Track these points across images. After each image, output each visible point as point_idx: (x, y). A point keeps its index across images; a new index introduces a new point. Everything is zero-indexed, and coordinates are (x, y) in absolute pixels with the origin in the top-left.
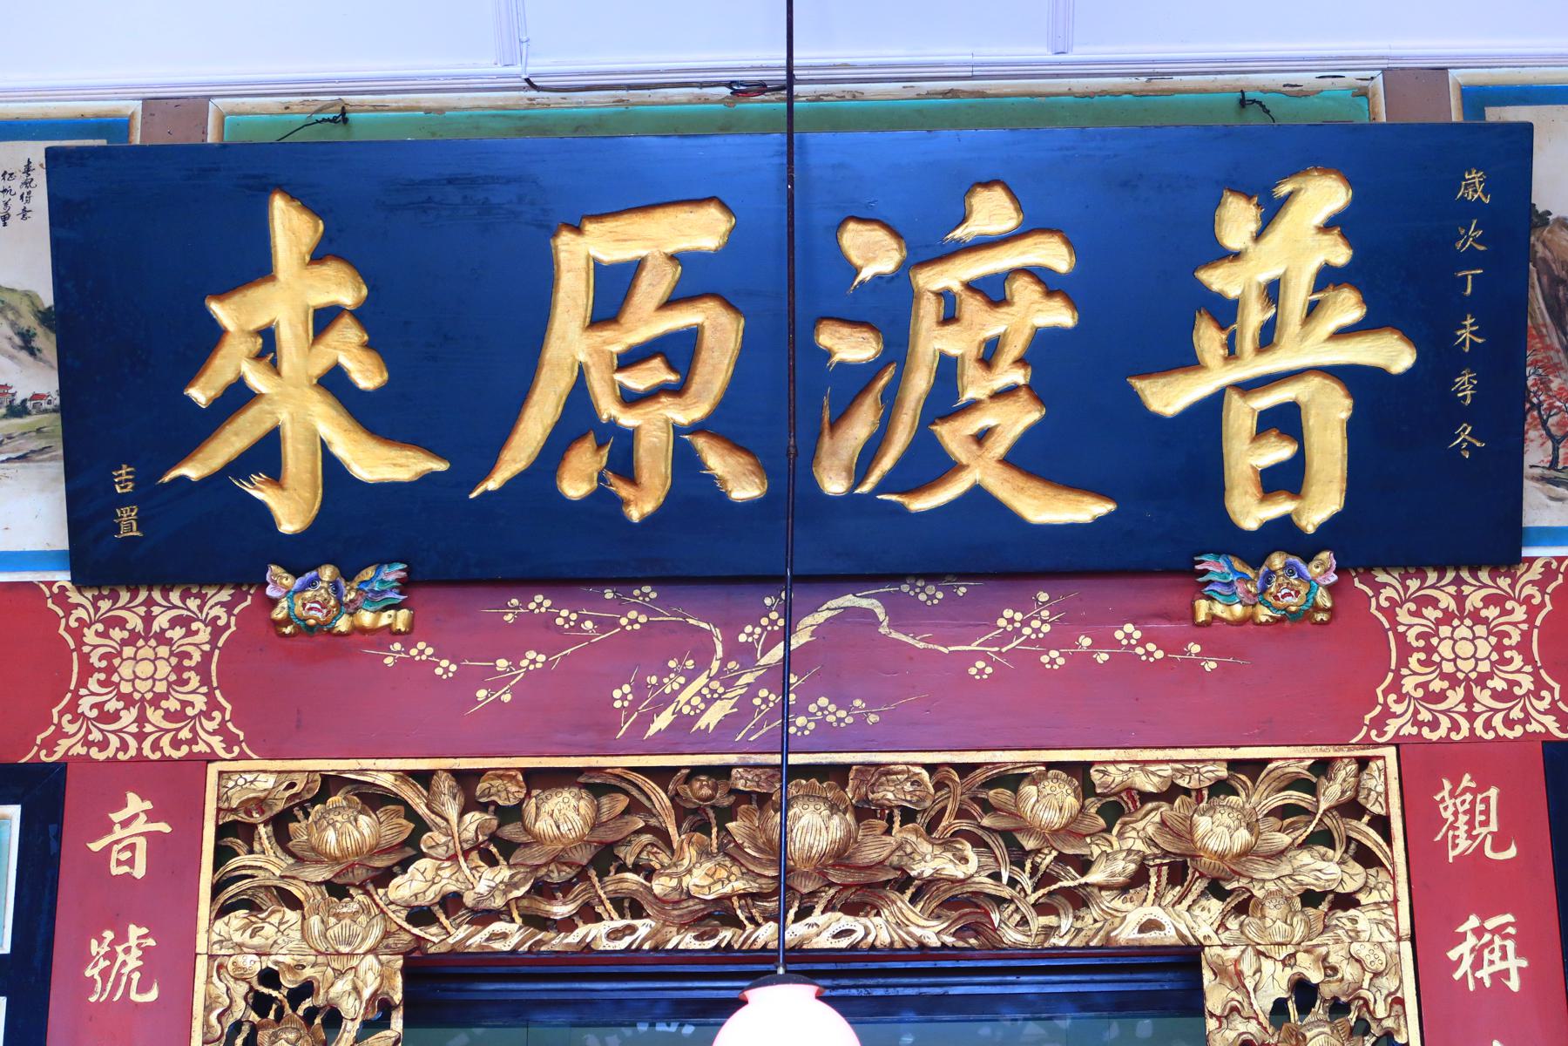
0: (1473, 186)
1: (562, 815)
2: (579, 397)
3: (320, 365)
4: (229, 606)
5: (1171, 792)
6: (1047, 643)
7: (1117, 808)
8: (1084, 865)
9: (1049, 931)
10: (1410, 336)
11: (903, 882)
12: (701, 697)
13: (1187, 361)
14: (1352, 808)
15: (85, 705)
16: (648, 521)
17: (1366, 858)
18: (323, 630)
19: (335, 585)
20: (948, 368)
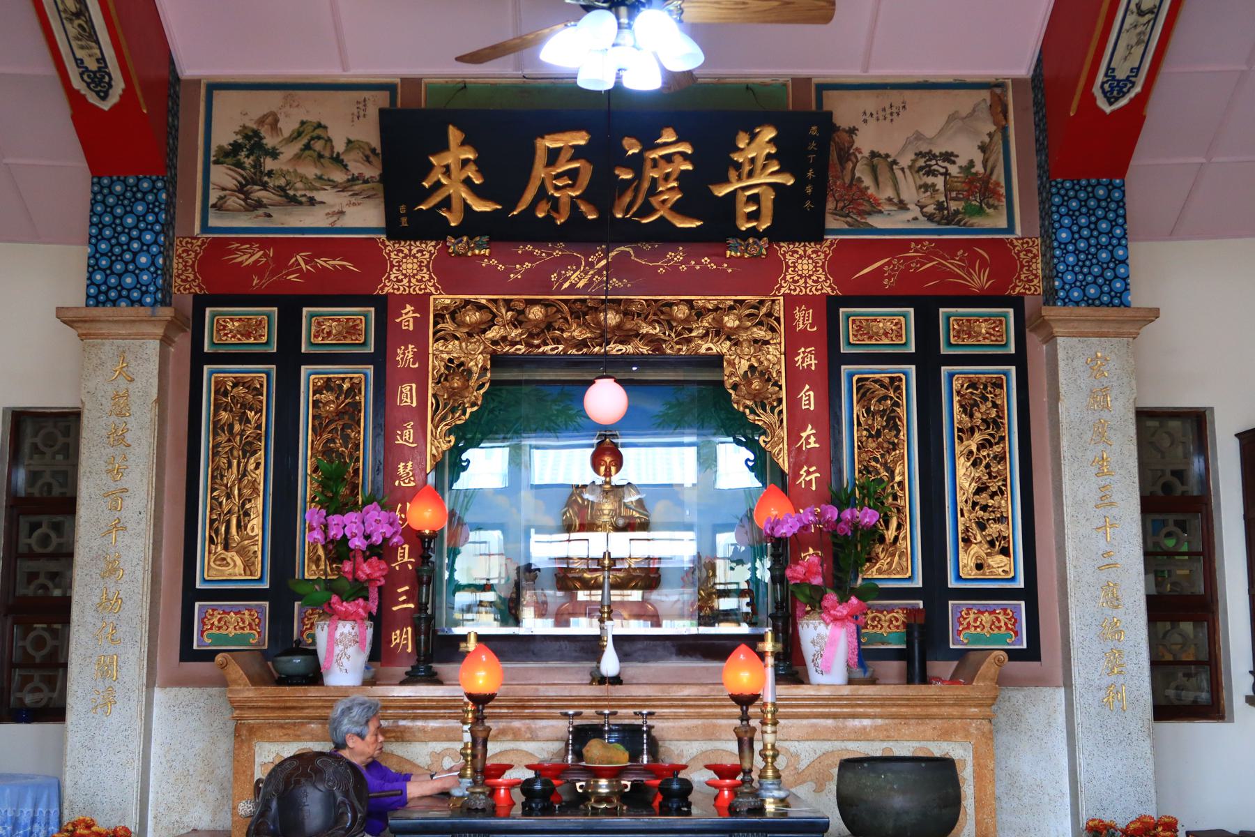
0: (814, 130)
1: (536, 313)
2: (542, 188)
3: (463, 177)
4: (434, 247)
5: (717, 309)
6: (682, 263)
7: (700, 313)
8: (691, 331)
9: (680, 350)
10: (793, 174)
11: (637, 335)
12: (577, 278)
13: (726, 181)
14: (769, 315)
15: (392, 277)
16: (562, 224)
17: (773, 330)
18: (465, 255)
19: (468, 243)
20: (654, 180)
